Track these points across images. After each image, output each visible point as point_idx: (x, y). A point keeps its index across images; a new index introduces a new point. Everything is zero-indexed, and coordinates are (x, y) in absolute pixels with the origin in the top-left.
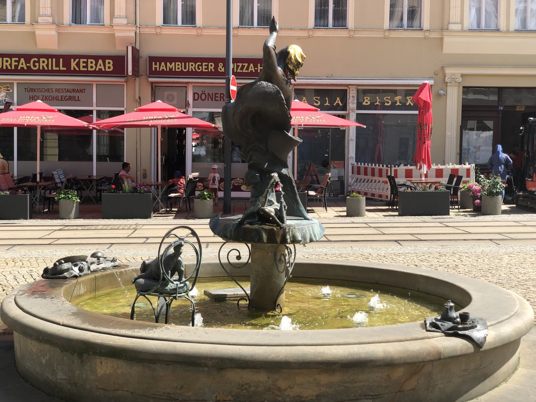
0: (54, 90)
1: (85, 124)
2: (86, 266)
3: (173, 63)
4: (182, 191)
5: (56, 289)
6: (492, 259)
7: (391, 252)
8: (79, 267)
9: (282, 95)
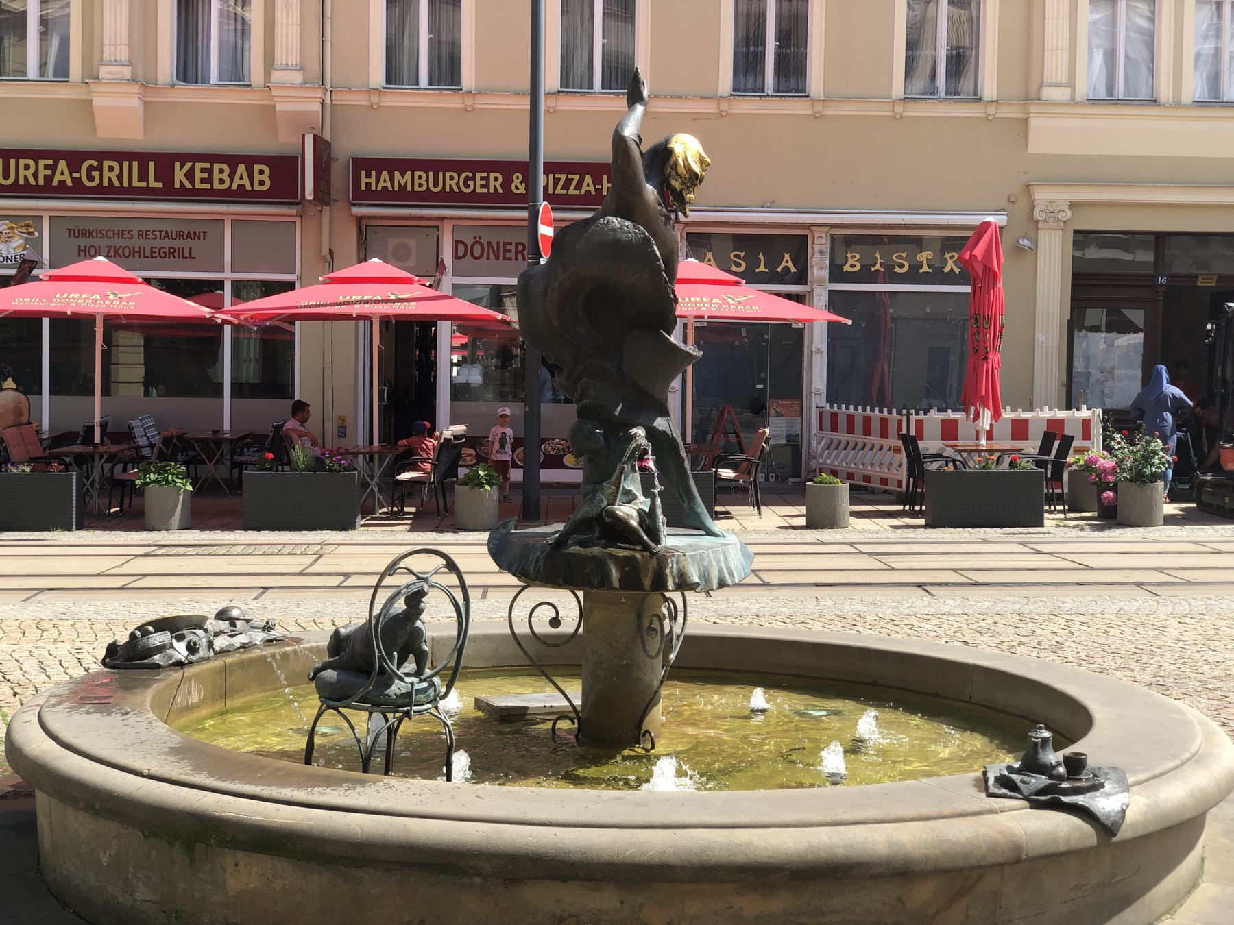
0: (135, 233)
1: (206, 311)
2: (204, 640)
3: (409, 174)
4: (428, 466)
5: (135, 693)
6: (1140, 629)
7: (907, 611)
8: (189, 643)
9: (656, 248)
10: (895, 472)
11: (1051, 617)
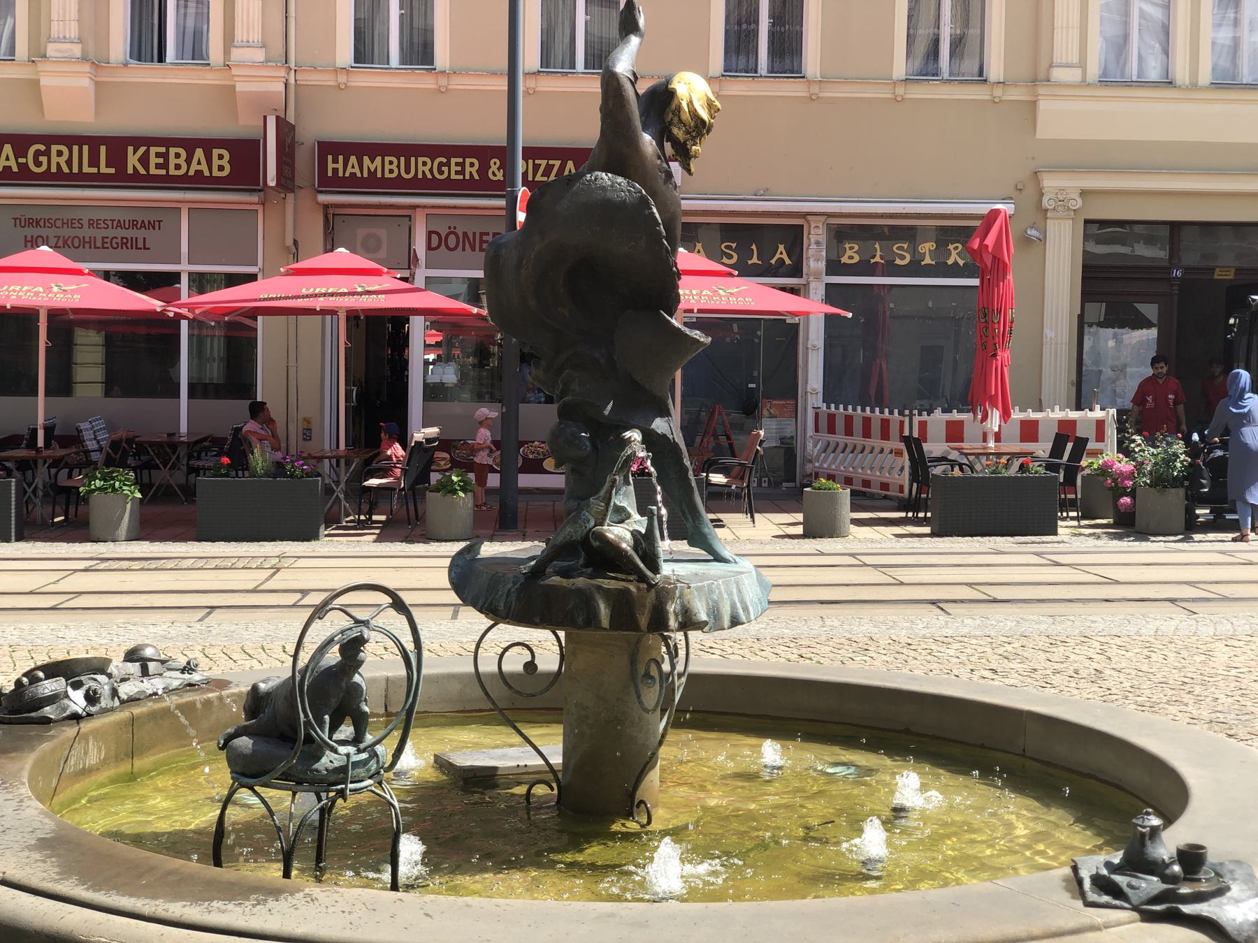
0: (85, 223)
1: (157, 305)
2: (106, 687)
3: (379, 159)
4: (398, 472)
5: (13, 758)
6: (1184, 653)
7: (923, 632)
8: (88, 691)
9: (655, 210)
10: (897, 476)
11: (1083, 639)
